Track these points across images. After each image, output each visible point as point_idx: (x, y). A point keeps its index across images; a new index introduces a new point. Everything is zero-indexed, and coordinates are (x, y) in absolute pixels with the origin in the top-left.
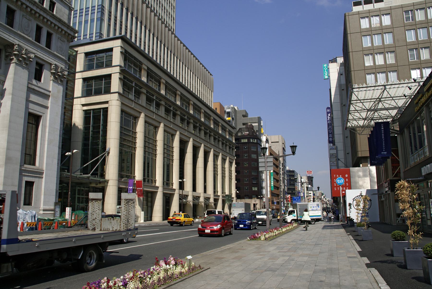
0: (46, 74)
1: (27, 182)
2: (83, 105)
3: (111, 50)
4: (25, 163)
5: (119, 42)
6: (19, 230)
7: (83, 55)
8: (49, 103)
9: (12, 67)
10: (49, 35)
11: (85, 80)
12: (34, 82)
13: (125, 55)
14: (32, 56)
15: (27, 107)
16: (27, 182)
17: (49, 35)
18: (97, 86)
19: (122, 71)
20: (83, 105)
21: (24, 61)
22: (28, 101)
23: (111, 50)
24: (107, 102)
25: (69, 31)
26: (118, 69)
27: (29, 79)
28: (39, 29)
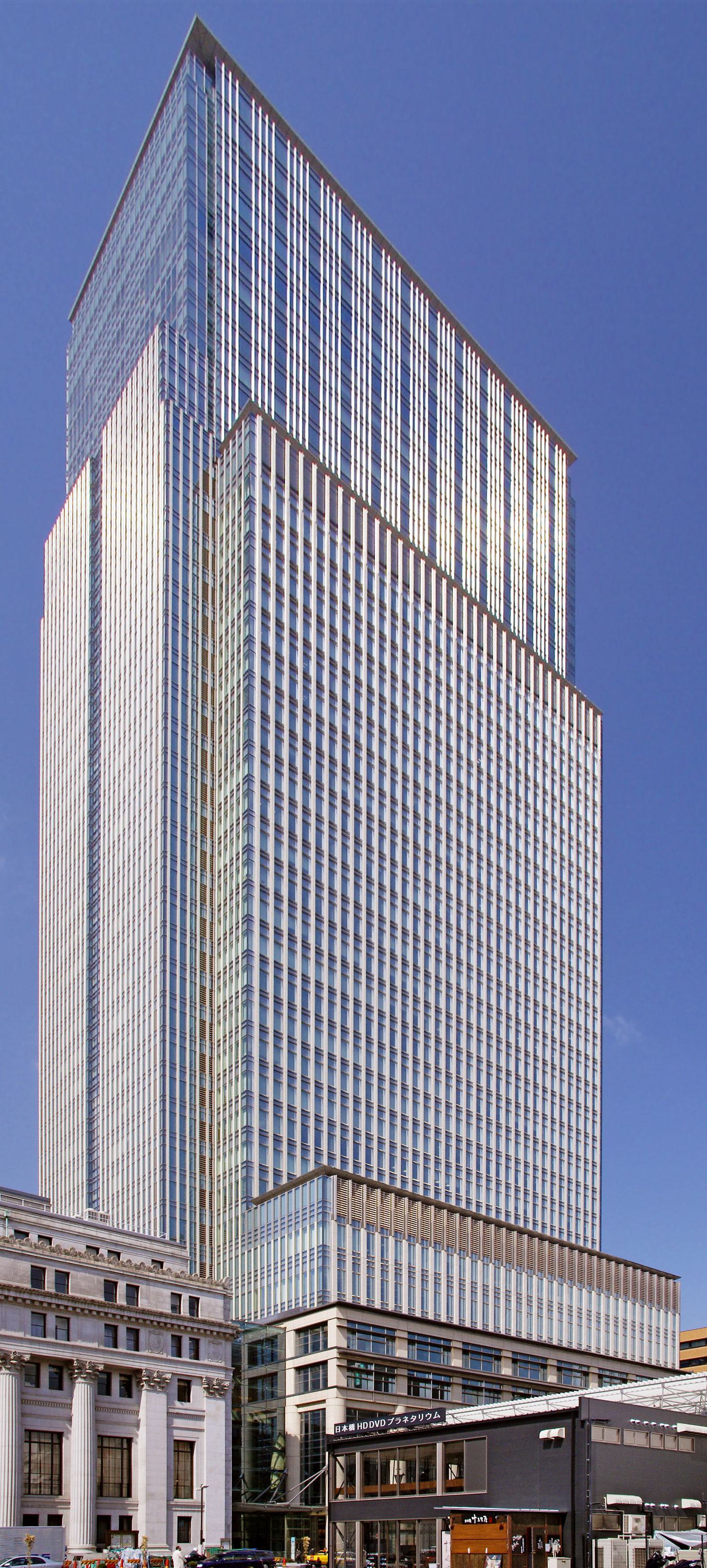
0: (197, 1391)
1: (180, 1518)
2: (298, 1406)
3: (325, 1324)
4: (177, 1496)
5: (334, 1312)
6: (611, 1499)
7: (293, 1333)
8: (204, 1425)
9: (144, 1393)
10: (195, 1343)
11: (298, 1369)
12: (178, 1404)
13: (350, 1329)
14: (169, 1376)
15: (169, 1435)
16: (180, 1518)
17: (195, 1343)
18: (312, 1376)
19: (344, 1354)
20: (298, 1406)
21: (159, 1384)
22: (170, 1427)
23: (325, 1324)
24: (324, 1401)
25: (223, 1330)
26: (334, 1353)
27: (169, 1403)
28: (177, 1340)
